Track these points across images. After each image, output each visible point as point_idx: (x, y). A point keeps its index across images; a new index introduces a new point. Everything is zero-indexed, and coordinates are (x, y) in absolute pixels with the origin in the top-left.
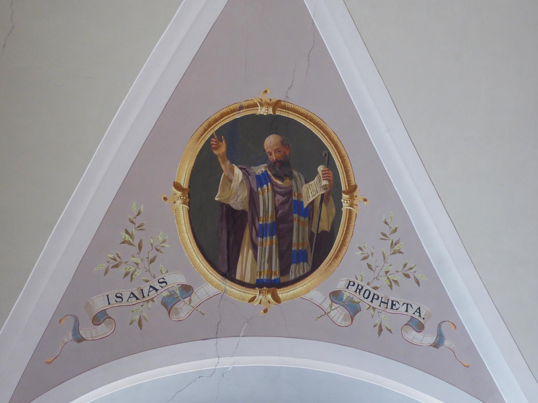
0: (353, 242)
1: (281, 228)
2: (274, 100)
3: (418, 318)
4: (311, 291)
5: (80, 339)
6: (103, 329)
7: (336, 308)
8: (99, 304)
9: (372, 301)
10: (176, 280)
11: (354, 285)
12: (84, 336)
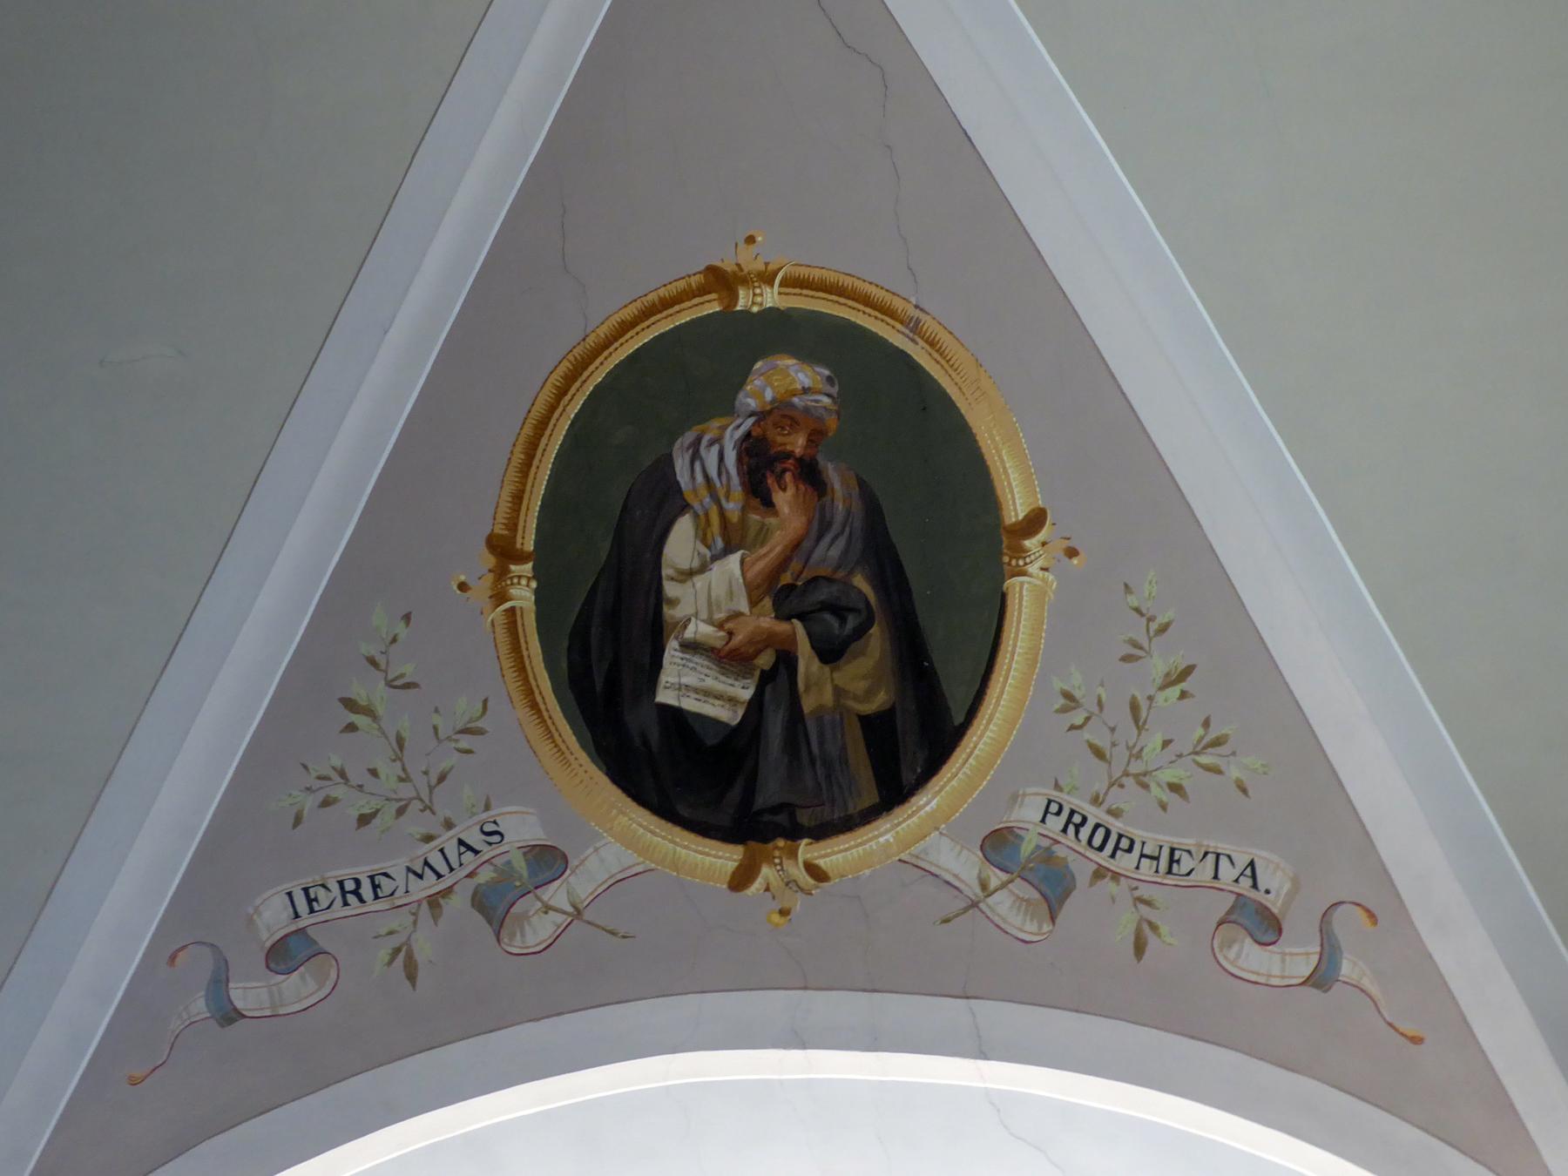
2: (490, 561)
3: (1252, 894)
5: (229, 1016)
6: (298, 988)
7: (1004, 886)
8: (273, 918)
9: (1113, 856)
11: (1058, 813)
12: (239, 1004)
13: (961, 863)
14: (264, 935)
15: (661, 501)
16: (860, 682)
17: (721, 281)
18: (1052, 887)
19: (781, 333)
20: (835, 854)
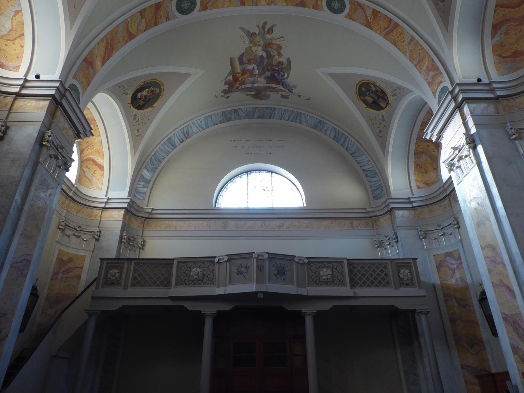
0: (385, 89)
1: (379, 97)
4: (391, 99)
5: (381, 137)
6: (382, 133)
8: (378, 131)
10: (380, 117)
13: (134, 114)
14: (481, 195)
15: (149, 87)
16: (141, 102)
17: (163, 84)
18: (135, 119)
19: (160, 89)
20: (132, 107)
